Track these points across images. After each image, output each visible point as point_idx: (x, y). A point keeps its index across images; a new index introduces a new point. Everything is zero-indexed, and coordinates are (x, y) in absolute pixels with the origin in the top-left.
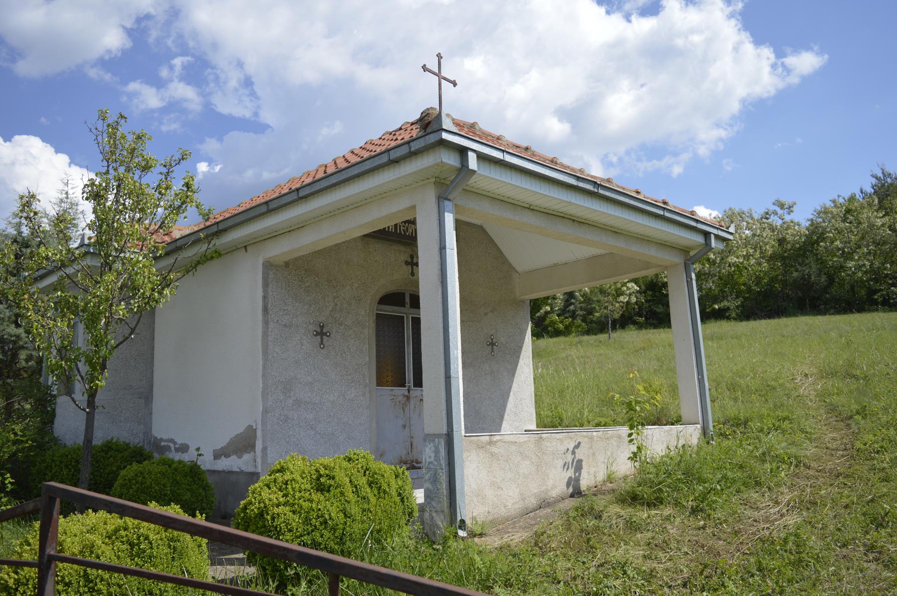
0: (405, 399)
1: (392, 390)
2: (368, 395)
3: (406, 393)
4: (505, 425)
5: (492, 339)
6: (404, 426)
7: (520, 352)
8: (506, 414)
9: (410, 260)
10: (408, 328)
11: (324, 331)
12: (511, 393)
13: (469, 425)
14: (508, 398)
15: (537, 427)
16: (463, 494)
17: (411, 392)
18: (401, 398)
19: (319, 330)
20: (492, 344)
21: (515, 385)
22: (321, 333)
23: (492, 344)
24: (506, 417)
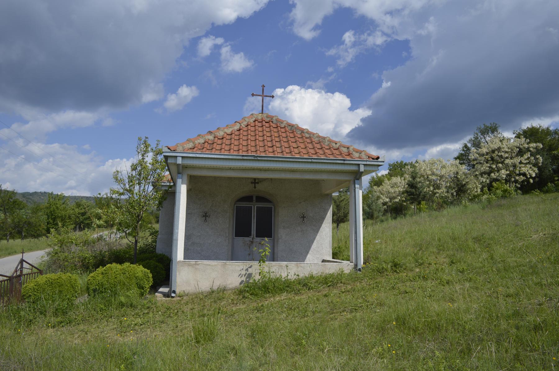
0: (251, 243)
1: (243, 239)
2: (227, 241)
3: (251, 240)
4: (309, 256)
5: (304, 215)
6: (249, 254)
7: (323, 221)
8: (310, 251)
9: (254, 181)
10: (254, 211)
11: (207, 215)
12: (315, 241)
13: (365, 252)
14: (313, 243)
15: (333, 258)
16: (176, 282)
17: (254, 240)
18: (248, 242)
19: (204, 215)
20: (303, 217)
21: (318, 237)
22: (206, 216)
23: (303, 217)
24: (310, 252)
